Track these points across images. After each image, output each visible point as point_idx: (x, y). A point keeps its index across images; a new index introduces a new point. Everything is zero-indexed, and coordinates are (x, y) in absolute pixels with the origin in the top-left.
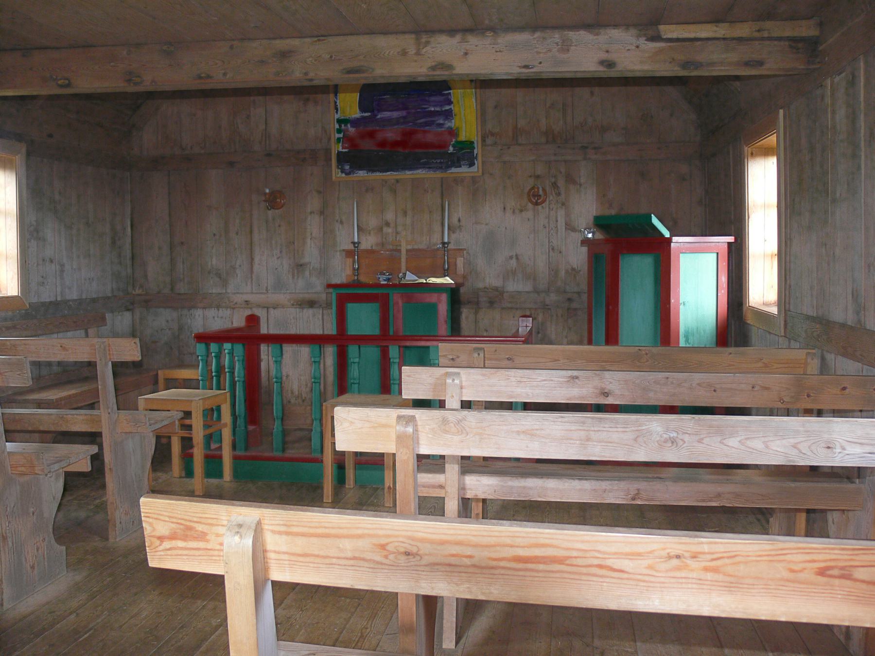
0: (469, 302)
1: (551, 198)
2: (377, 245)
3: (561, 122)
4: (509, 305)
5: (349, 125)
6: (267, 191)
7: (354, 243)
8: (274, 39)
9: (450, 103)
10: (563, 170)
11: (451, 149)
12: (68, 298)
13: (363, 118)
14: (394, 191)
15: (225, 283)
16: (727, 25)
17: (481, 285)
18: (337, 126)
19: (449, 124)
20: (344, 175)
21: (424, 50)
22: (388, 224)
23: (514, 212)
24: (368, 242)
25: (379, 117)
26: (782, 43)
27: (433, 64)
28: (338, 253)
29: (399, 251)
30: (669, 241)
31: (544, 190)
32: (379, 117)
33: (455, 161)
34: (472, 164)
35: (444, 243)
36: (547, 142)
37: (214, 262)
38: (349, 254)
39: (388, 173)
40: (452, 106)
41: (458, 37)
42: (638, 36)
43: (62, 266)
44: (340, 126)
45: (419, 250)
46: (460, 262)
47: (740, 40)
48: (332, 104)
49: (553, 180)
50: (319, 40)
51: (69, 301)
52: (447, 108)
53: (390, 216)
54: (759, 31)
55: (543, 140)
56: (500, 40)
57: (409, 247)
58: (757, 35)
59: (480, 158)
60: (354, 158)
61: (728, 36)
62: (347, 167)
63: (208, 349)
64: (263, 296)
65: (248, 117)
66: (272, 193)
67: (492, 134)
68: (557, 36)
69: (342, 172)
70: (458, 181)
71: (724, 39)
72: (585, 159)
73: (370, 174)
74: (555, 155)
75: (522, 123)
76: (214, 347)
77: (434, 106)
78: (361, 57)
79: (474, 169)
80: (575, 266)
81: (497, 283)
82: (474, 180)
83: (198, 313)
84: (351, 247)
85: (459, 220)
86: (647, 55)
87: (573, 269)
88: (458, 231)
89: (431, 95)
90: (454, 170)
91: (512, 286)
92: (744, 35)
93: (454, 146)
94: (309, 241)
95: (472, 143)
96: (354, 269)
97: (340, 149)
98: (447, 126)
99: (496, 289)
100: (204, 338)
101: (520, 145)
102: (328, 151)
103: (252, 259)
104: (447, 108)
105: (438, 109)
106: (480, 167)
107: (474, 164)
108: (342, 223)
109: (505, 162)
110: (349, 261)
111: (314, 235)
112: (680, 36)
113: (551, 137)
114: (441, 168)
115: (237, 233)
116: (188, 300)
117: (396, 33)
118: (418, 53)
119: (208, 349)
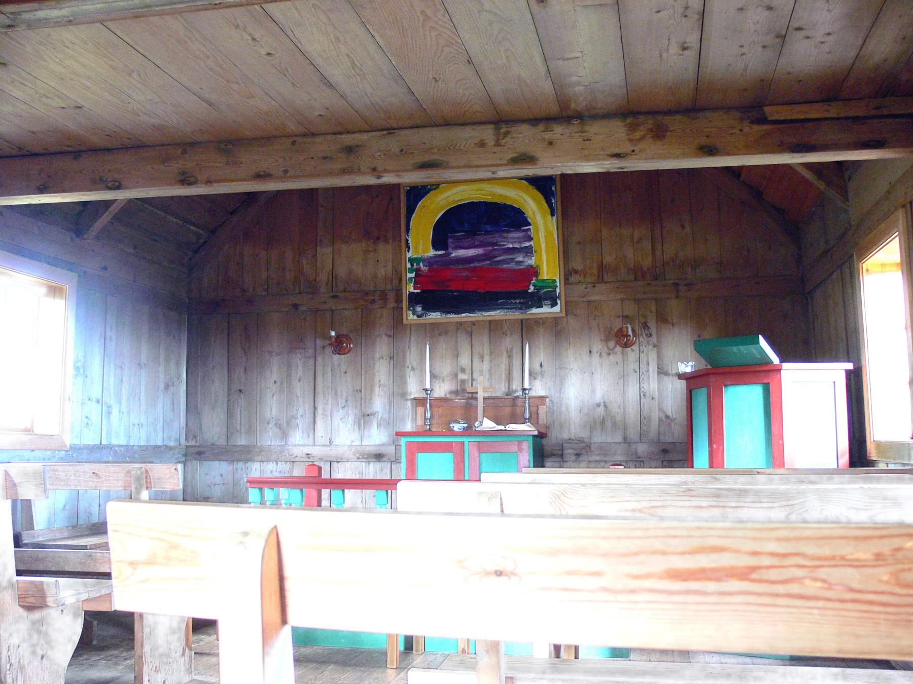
0: (552, 455)
1: (641, 339)
2: (451, 392)
3: (650, 258)
4: (598, 458)
5: (421, 265)
6: (333, 334)
7: (426, 390)
8: (340, 133)
9: (530, 239)
10: (653, 309)
11: (532, 289)
12: (114, 442)
13: (436, 256)
14: (471, 334)
15: (285, 435)
16: (841, 103)
17: (565, 436)
18: (409, 266)
19: (530, 262)
20: (415, 317)
21: (504, 141)
22: (463, 370)
23: (600, 355)
24: (442, 390)
25: (453, 255)
26: (903, 120)
27: (515, 155)
28: (409, 403)
29: (476, 399)
30: (778, 370)
31: (633, 330)
32: (453, 255)
33: (537, 300)
34: (554, 304)
35: (524, 390)
36: (636, 279)
37: (274, 412)
38: (420, 402)
39: (464, 315)
40: (532, 243)
41: (541, 127)
42: (741, 119)
43: (110, 407)
44: (412, 265)
45: (497, 398)
46: (542, 410)
47: (856, 119)
48: (403, 242)
49: (643, 321)
50: (389, 134)
51: (115, 446)
52: (527, 244)
53: (464, 361)
54: (876, 108)
55: (631, 277)
56: (587, 128)
57: (487, 395)
58: (873, 112)
59: (563, 297)
60: (429, 299)
61: (843, 115)
62: (419, 309)
63: (262, 496)
64: (325, 448)
65: (315, 256)
66: (338, 337)
67: (576, 272)
68: (650, 122)
69: (414, 314)
70: (539, 322)
71: (838, 119)
72: (677, 297)
73: (444, 316)
74: (644, 292)
75: (608, 259)
76: (267, 491)
77: (512, 243)
78: (435, 150)
79: (557, 309)
80: (669, 414)
81: (584, 434)
82: (556, 320)
83: (257, 465)
84: (422, 395)
85: (541, 365)
86: (752, 139)
87: (667, 417)
88: (539, 377)
89: (509, 232)
90: (535, 310)
91: (599, 438)
92: (861, 114)
93: (535, 286)
94: (377, 389)
95: (554, 281)
96: (426, 419)
97: (412, 290)
98: (526, 264)
99: (581, 441)
100: (253, 482)
101: (606, 282)
102: (398, 293)
103: (315, 408)
104: (527, 244)
105: (517, 246)
106: (564, 307)
107: (557, 304)
108: (413, 369)
109: (589, 302)
110: (420, 410)
111: (382, 382)
112: (789, 118)
113: (638, 273)
114: (521, 309)
115: (299, 380)
116: (246, 454)
117: (474, 124)
118: (497, 144)
119: (262, 496)
